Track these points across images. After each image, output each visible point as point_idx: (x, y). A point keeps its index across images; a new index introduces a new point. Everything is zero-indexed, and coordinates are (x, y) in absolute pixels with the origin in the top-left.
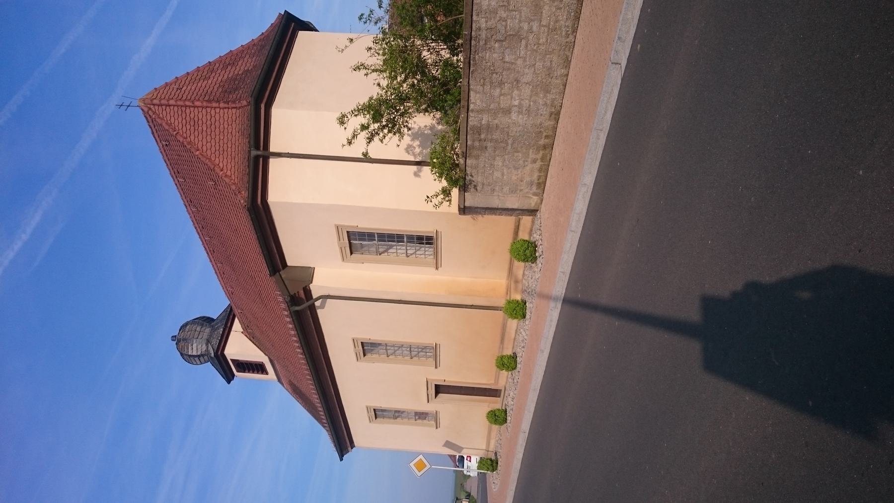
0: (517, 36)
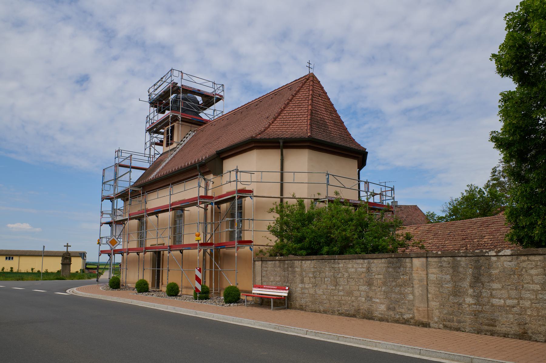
0: (337, 284)
